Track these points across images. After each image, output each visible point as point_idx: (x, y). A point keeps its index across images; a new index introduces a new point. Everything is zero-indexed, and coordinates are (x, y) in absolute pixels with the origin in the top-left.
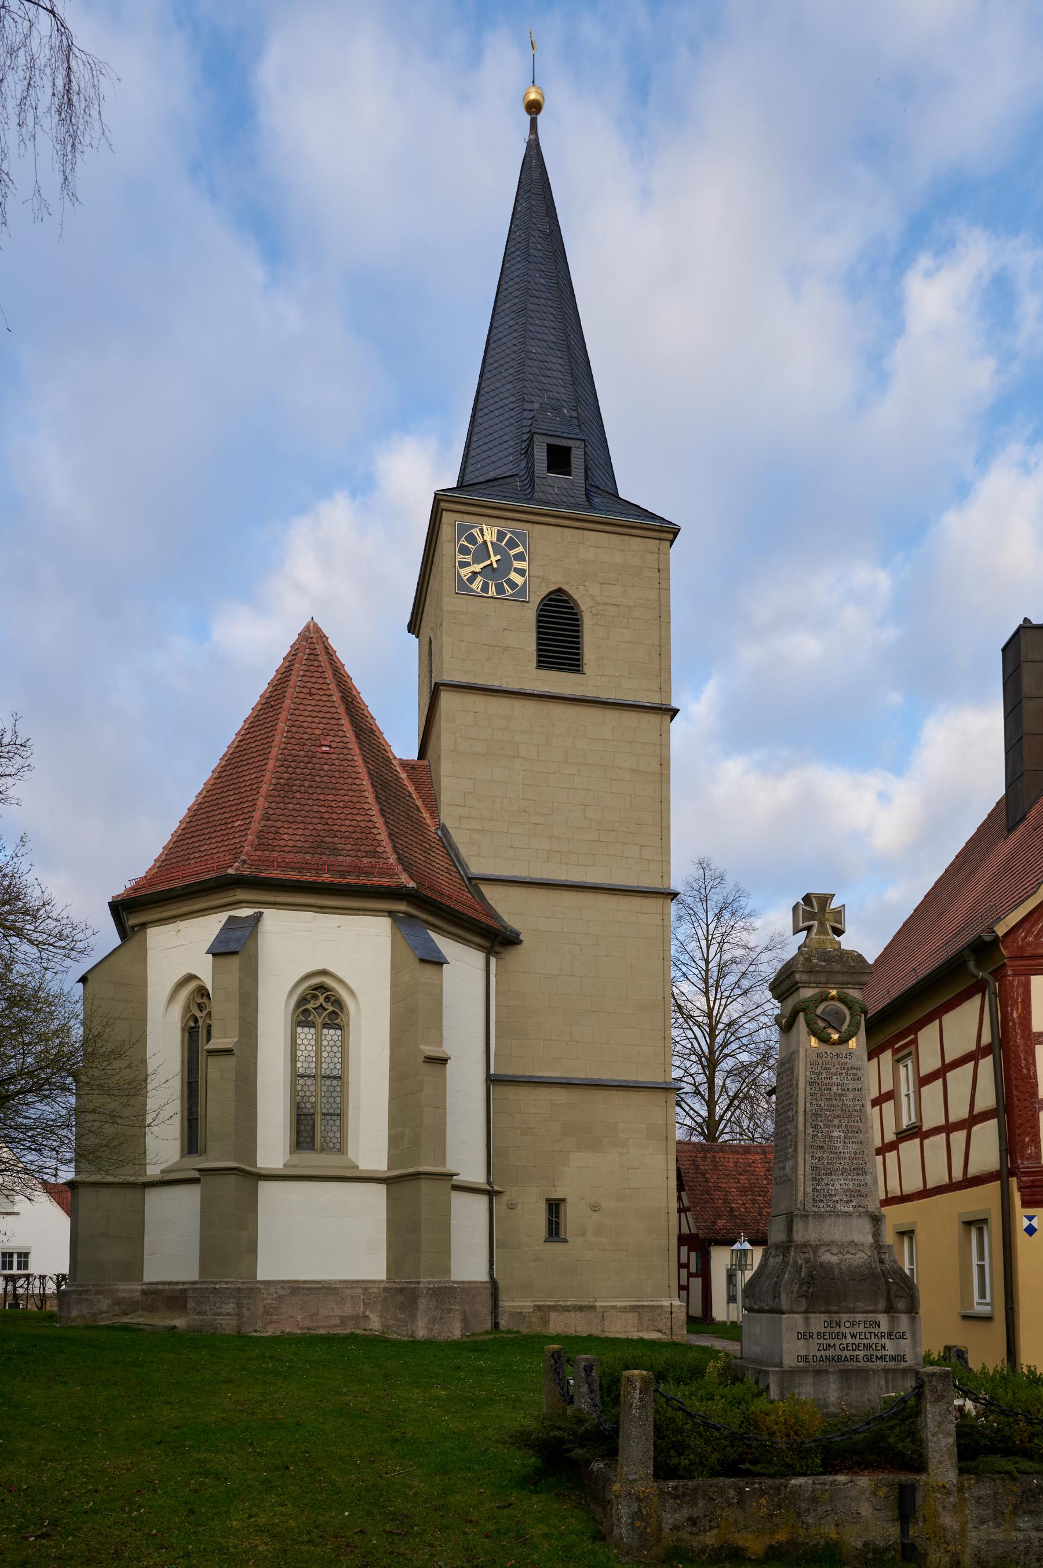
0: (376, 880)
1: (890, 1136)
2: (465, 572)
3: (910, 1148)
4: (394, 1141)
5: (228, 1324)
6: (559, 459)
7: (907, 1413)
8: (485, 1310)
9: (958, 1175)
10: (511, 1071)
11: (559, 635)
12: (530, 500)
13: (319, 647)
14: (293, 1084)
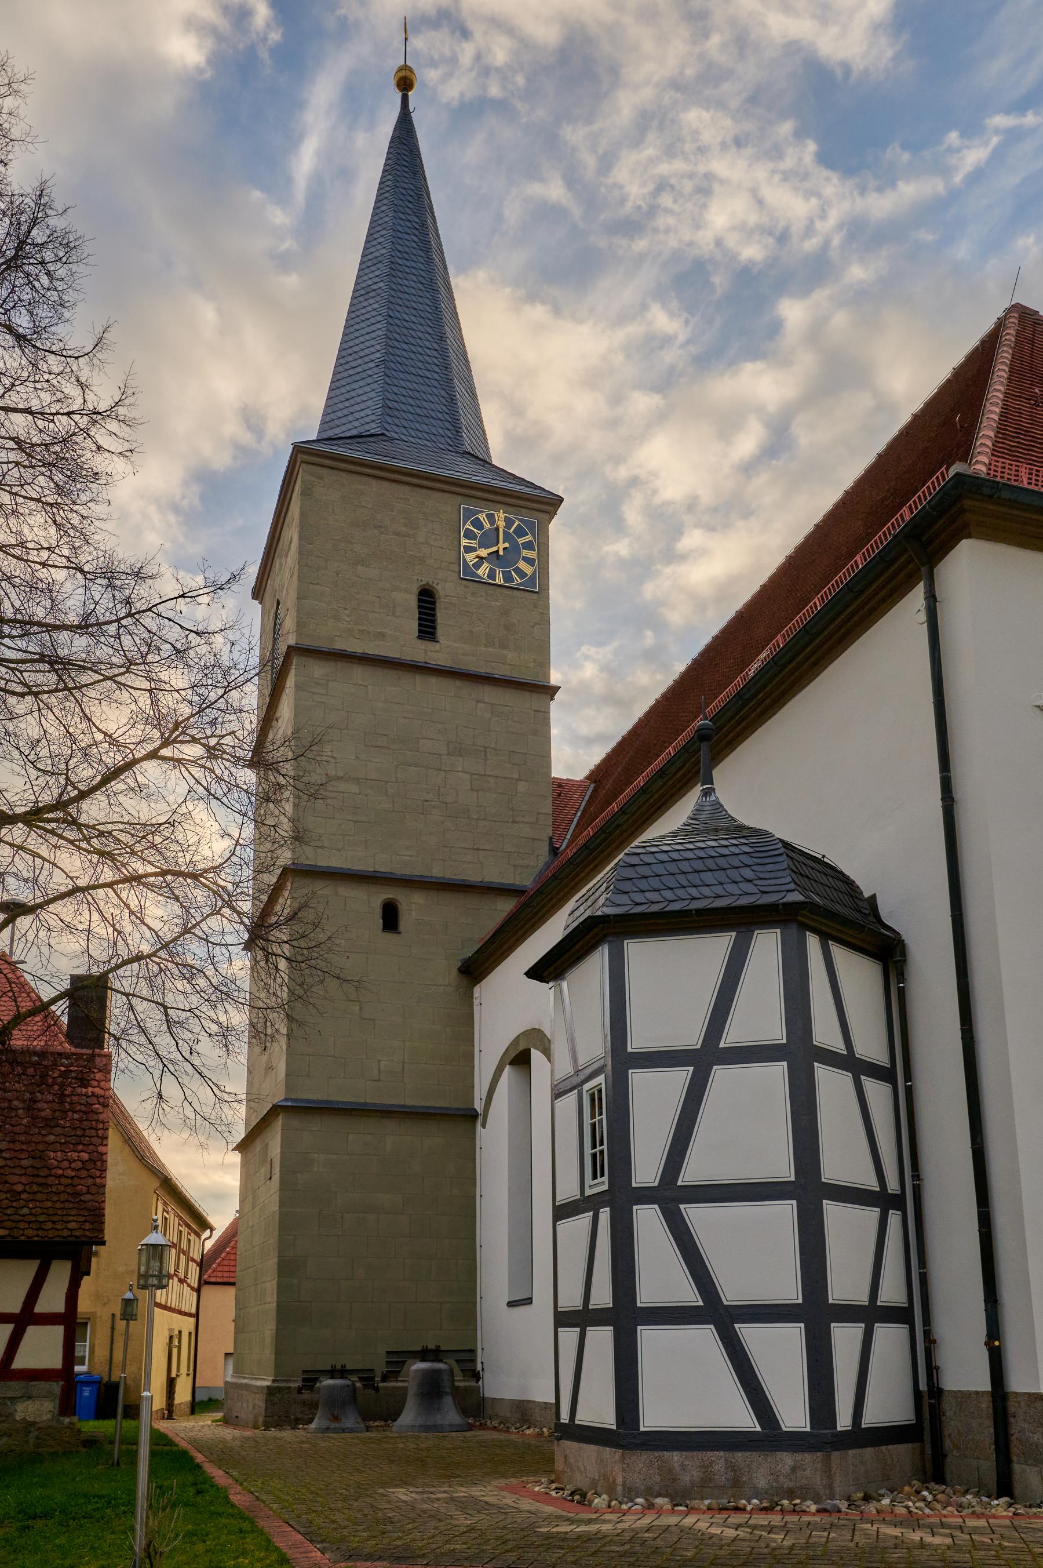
2: (471, 558)
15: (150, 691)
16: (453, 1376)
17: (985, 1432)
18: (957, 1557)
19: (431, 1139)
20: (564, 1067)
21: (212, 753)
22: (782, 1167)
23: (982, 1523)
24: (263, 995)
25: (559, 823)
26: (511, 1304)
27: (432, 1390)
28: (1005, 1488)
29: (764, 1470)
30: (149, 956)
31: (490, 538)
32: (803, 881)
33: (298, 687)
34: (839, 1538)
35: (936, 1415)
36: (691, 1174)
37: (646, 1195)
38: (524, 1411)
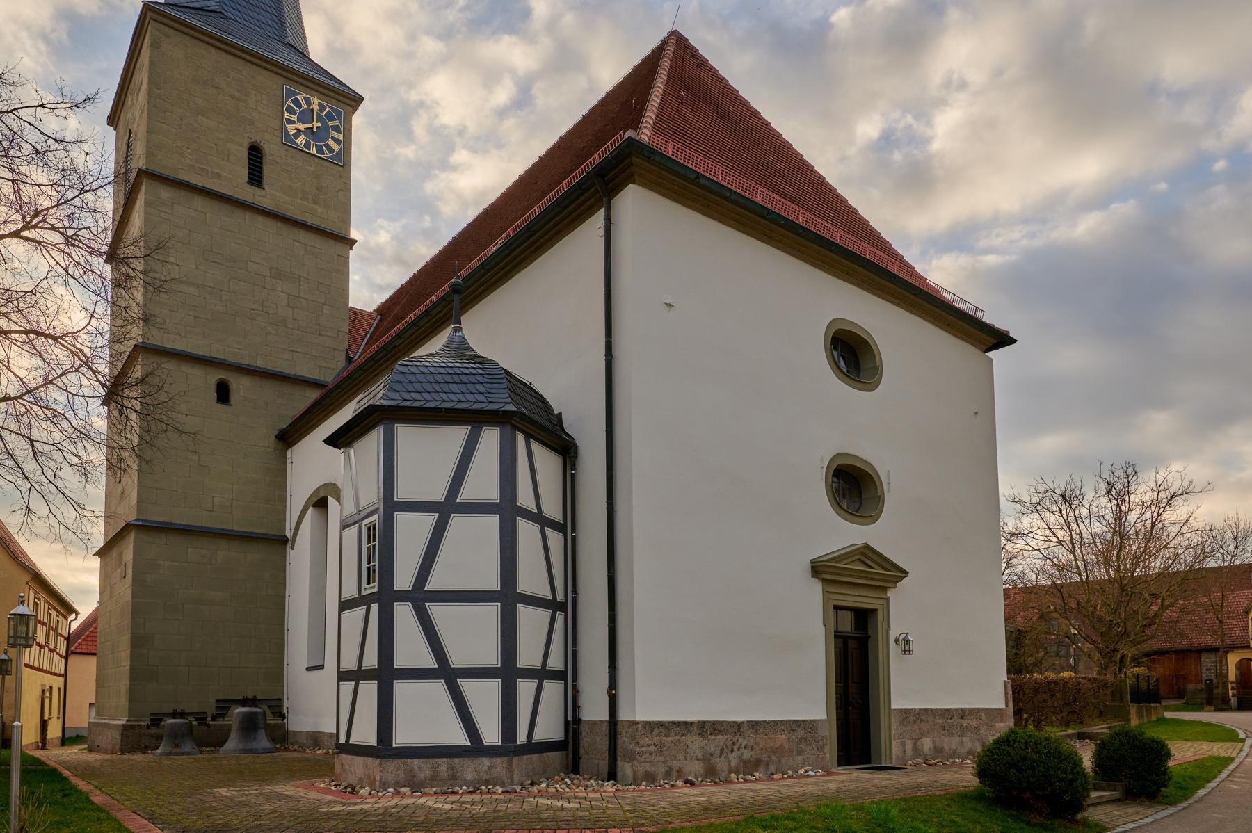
2: (291, 128)
15: (13, 181)
16: (265, 719)
17: (604, 745)
18: (581, 814)
20: (349, 507)
21: (71, 241)
22: (492, 581)
23: (598, 795)
24: (115, 437)
25: (353, 338)
26: (308, 669)
27: (250, 726)
28: (612, 776)
29: (471, 769)
30: (16, 398)
31: (306, 116)
32: (516, 398)
33: (148, 204)
34: (515, 807)
35: (577, 734)
36: (433, 584)
37: (403, 596)
38: (316, 739)
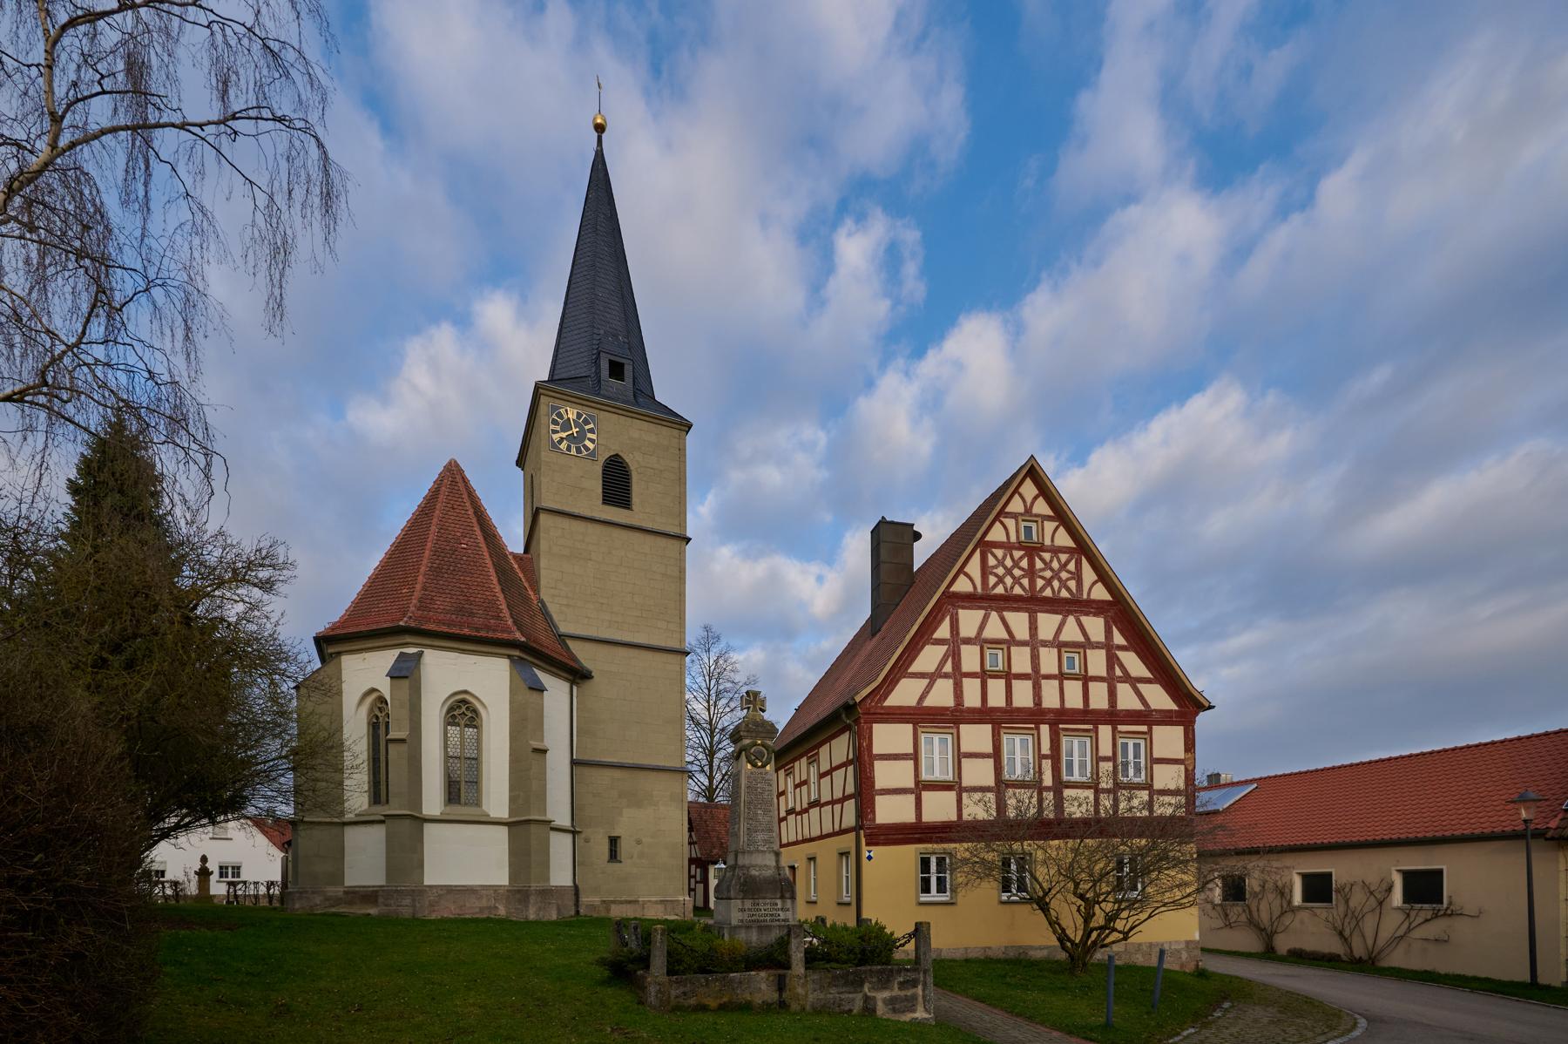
0: (499, 635)
1: (805, 805)
2: (556, 437)
3: (814, 812)
4: (513, 799)
5: (406, 912)
6: (617, 370)
7: (783, 944)
8: (571, 903)
9: (837, 828)
10: (586, 758)
11: (617, 482)
12: (598, 395)
13: (458, 478)
14: (446, 762)
19: (673, 545)
